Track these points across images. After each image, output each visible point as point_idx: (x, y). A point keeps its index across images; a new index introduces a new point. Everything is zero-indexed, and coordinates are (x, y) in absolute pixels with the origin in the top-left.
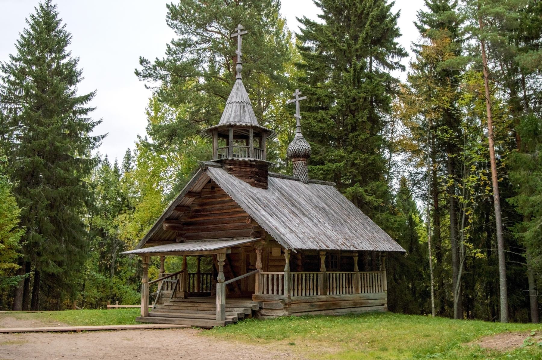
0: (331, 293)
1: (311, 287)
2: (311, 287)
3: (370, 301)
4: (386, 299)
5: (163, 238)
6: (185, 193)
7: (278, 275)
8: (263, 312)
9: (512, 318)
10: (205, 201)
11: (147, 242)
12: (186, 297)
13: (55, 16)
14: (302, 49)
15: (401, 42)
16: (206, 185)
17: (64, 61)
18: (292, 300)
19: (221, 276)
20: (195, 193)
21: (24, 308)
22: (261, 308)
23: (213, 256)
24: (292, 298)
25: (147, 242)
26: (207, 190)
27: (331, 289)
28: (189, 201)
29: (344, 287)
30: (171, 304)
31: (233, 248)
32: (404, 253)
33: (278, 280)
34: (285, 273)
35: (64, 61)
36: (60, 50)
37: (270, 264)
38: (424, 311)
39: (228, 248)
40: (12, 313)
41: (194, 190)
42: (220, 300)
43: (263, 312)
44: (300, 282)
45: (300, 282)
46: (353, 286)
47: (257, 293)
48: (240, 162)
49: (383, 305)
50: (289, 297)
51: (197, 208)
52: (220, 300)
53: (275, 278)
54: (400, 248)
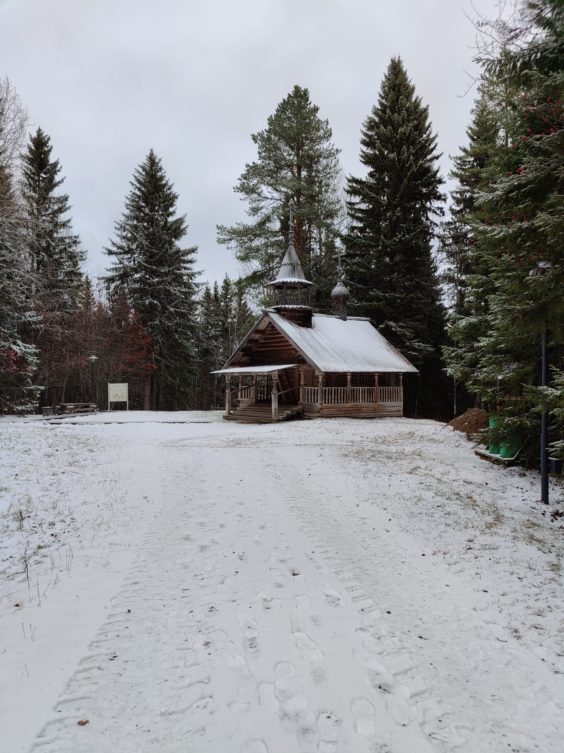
0: (355, 402)
1: (339, 398)
2: (339, 398)
3: (387, 408)
4: (402, 407)
5: (241, 361)
6: (253, 331)
7: (314, 389)
8: (305, 413)
9: (129, 410)
10: (267, 336)
11: (230, 365)
12: (256, 403)
13: (162, 178)
14: (350, 203)
15: (441, 189)
16: (268, 325)
17: (171, 219)
18: (323, 407)
19: (274, 391)
20: (260, 331)
21: (151, 409)
22: (304, 411)
23: (269, 376)
24: (324, 405)
25: (230, 365)
26: (269, 329)
27: (355, 399)
28: (257, 336)
29: (366, 398)
30: (246, 407)
31: (285, 370)
32: (417, 373)
33: (315, 393)
34: (319, 388)
35: (171, 219)
36: (166, 208)
37: (314, 380)
38: (126, 409)
39: (279, 371)
40: (255, 442)
41: (260, 329)
42: (274, 405)
43: (305, 413)
44: (330, 394)
45: (330, 394)
46: (374, 397)
47: (301, 401)
48: (291, 309)
49: (400, 411)
50: (321, 404)
51: (262, 341)
52: (274, 405)
53: (313, 391)
54: (414, 369)
